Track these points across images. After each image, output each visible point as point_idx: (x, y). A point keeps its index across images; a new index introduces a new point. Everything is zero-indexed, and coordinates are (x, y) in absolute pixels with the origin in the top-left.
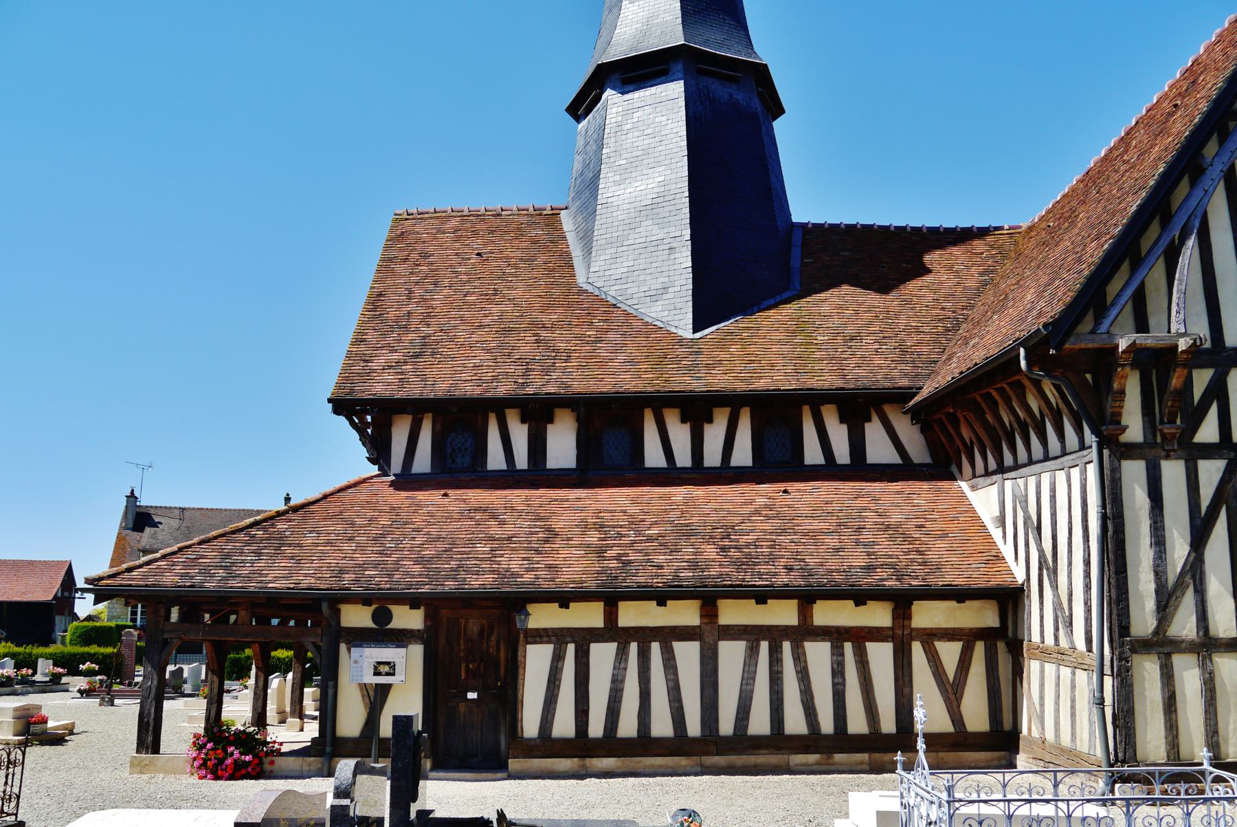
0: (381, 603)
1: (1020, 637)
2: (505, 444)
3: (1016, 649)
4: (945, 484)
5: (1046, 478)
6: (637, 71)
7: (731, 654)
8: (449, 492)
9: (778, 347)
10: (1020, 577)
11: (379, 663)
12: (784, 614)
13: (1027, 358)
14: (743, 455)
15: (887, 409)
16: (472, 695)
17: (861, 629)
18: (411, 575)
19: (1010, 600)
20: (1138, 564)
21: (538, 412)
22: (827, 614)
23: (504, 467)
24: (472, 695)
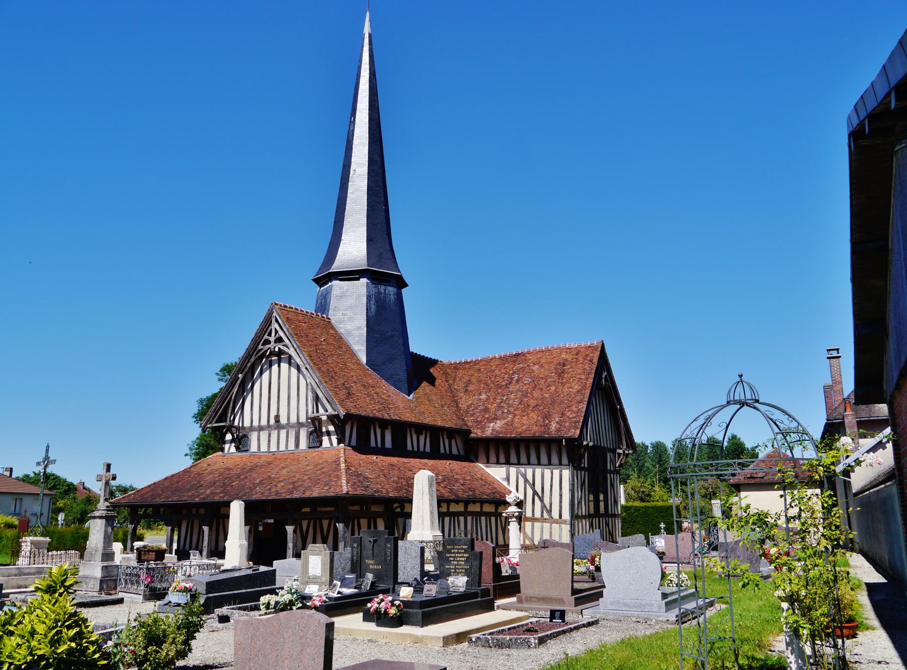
2: (444, 445)
4: (472, 464)
7: (469, 518)
22: (473, 508)
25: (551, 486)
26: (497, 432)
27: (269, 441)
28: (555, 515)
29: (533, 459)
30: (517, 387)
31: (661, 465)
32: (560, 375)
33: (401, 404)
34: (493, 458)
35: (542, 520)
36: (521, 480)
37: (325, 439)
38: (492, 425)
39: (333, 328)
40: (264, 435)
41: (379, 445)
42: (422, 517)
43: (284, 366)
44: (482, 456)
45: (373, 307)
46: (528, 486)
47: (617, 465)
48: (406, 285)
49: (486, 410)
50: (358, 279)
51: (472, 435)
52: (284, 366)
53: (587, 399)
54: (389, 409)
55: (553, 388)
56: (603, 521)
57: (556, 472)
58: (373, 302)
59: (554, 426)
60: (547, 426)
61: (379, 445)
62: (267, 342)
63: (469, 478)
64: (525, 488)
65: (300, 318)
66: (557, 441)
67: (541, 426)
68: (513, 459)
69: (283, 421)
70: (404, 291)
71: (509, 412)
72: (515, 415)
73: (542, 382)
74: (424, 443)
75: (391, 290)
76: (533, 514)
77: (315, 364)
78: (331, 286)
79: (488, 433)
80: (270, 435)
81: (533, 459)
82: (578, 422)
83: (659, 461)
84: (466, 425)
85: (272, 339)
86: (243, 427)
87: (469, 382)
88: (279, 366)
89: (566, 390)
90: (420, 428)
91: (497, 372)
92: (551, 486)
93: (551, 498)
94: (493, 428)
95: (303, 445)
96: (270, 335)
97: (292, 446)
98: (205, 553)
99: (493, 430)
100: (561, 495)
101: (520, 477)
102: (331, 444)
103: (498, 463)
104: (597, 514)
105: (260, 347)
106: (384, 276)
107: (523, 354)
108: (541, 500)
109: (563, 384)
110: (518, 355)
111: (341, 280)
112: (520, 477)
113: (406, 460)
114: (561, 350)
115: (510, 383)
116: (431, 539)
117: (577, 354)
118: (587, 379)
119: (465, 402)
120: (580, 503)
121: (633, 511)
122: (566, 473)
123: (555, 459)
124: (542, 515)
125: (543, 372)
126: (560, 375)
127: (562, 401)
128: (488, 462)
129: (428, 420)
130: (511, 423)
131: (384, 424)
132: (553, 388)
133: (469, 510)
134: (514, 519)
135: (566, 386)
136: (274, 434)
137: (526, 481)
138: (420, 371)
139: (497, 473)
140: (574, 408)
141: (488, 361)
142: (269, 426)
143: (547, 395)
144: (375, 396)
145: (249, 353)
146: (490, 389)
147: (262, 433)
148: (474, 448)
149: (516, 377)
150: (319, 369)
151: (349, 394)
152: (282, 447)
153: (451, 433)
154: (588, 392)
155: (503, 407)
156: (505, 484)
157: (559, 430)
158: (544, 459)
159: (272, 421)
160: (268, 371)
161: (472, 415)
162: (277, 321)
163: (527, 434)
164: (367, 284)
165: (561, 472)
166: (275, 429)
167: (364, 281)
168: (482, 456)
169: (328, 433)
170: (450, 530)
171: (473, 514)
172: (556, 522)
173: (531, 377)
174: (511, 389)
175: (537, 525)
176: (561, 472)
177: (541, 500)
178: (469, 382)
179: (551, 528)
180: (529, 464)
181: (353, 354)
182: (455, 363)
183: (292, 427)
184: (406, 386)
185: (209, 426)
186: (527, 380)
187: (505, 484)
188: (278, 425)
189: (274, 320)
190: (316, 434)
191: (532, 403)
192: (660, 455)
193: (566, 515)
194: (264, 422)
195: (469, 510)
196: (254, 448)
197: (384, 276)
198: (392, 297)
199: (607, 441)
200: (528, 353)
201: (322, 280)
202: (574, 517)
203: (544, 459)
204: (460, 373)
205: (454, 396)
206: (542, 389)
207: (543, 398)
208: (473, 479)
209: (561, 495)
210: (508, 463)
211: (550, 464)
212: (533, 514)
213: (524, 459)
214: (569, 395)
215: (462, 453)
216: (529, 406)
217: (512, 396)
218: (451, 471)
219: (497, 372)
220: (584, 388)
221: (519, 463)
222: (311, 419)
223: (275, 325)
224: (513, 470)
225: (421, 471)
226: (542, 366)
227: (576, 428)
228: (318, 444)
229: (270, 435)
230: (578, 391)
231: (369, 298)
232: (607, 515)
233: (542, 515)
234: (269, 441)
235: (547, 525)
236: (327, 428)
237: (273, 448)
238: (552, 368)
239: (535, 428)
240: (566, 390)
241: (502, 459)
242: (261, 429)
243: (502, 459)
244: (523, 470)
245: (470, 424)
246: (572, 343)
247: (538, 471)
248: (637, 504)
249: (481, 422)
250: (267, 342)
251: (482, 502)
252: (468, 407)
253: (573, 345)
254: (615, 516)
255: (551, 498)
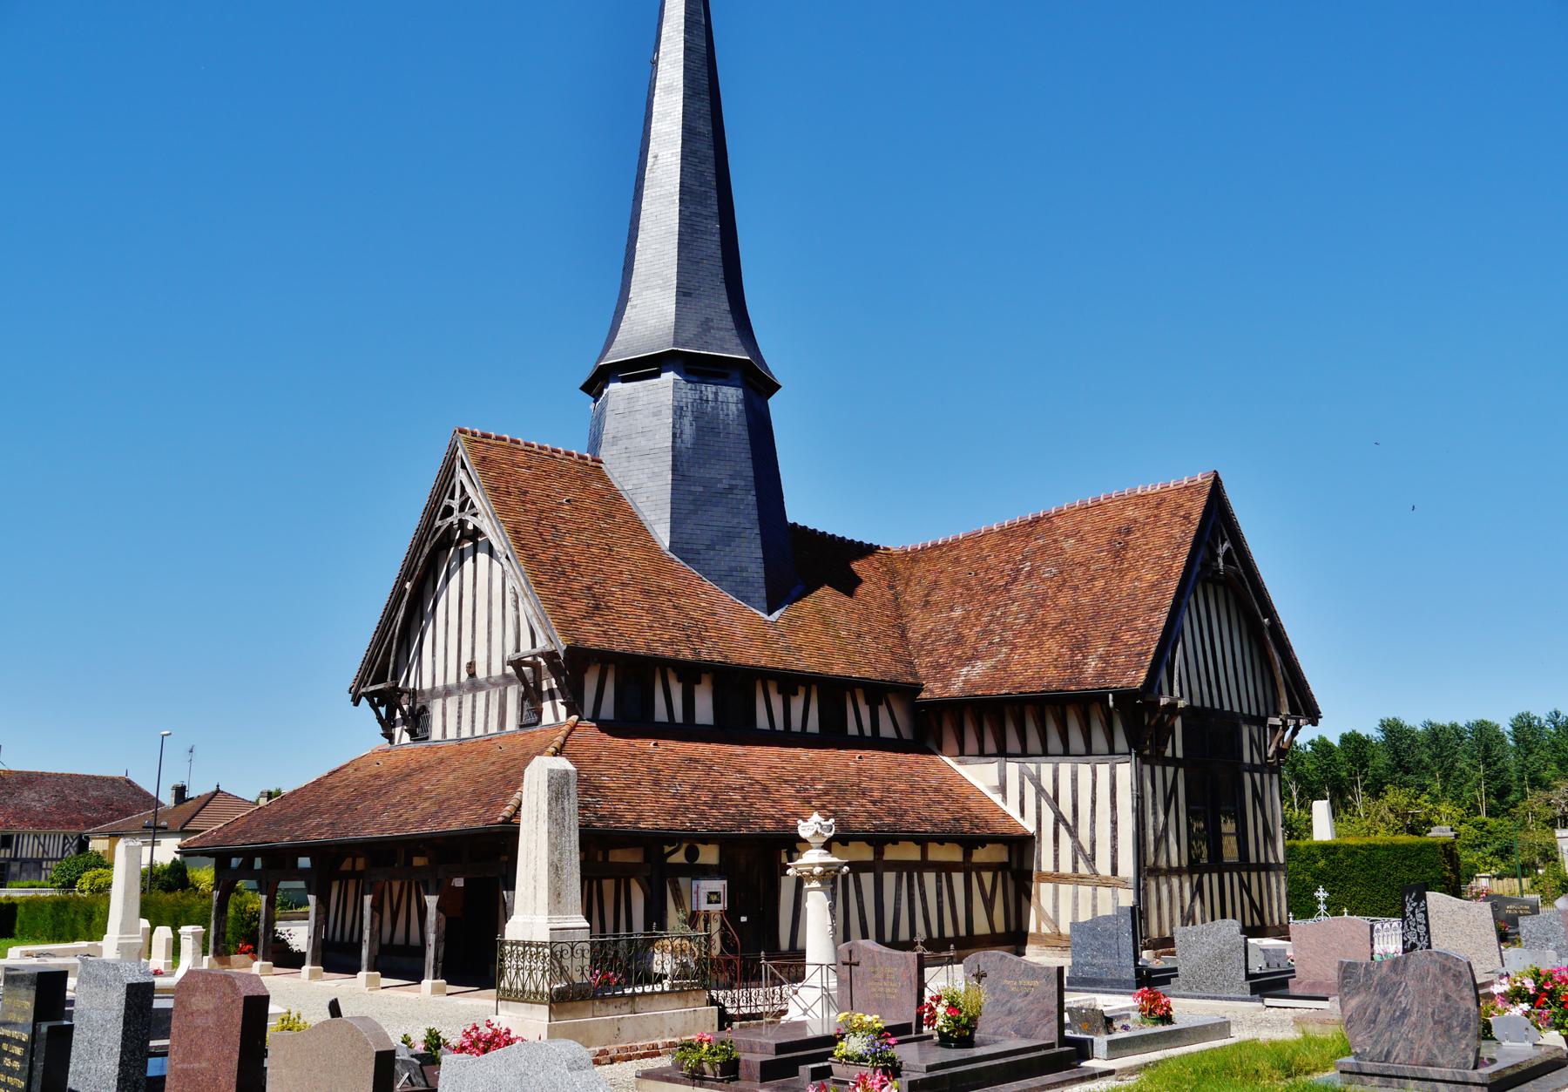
0: (693, 840)
1: (1026, 867)
2: (857, 717)
3: (1028, 875)
4: (925, 758)
5: (451, 734)
6: (642, 368)
7: (889, 878)
9: (746, 631)
10: (1032, 829)
15: (670, 671)
18: (715, 820)
19: (1022, 845)
20: (127, 893)
22: (938, 853)
25: (1094, 802)
26: (975, 686)
27: (460, 717)
28: (1103, 867)
29: (1054, 743)
31: (1488, 766)
32: (1118, 555)
33: (739, 630)
34: (971, 743)
35: (1076, 879)
36: (1030, 791)
37: (547, 706)
40: (452, 702)
41: (679, 718)
42: (535, 878)
43: (483, 557)
44: (950, 741)
45: (688, 430)
47: (1270, 752)
48: (775, 387)
49: (959, 640)
50: (656, 375)
51: (923, 695)
52: (483, 557)
53: (1170, 602)
55: (1100, 583)
56: (1232, 880)
57: (1103, 771)
58: (687, 421)
59: (1092, 665)
60: (1077, 667)
61: (679, 718)
62: (449, 511)
63: (902, 787)
64: (1039, 808)
65: (520, 458)
66: (1099, 697)
67: (1065, 667)
68: (1013, 744)
69: (481, 673)
71: (1003, 642)
72: (1015, 647)
73: (1079, 572)
74: (805, 713)
75: (731, 395)
79: (956, 689)
81: (1054, 743)
83: (1484, 759)
84: (915, 675)
85: (455, 504)
86: (422, 692)
88: (475, 560)
89: (1126, 586)
90: (789, 682)
91: (992, 561)
92: (1094, 802)
93: (1093, 829)
94: (967, 678)
95: (512, 724)
96: (452, 497)
97: (493, 728)
98: (260, 952)
99: (965, 682)
100: (1114, 823)
101: (1027, 783)
102: (557, 718)
103: (982, 754)
104: (1217, 864)
105: (438, 523)
106: (726, 373)
107: (1048, 518)
108: (1073, 832)
110: (1037, 520)
111: (624, 380)
112: (1027, 783)
113: (739, 750)
114: (1125, 501)
115: (1015, 580)
117: (1158, 506)
118: (1175, 556)
119: (920, 624)
120: (1161, 838)
122: (1125, 772)
123: (1099, 741)
124: (1075, 869)
125: (1084, 551)
126: (1118, 555)
128: (962, 753)
129: (806, 663)
130: (1006, 664)
131: (690, 673)
132: (1100, 583)
134: (816, 884)
135: (1127, 578)
136: (468, 699)
137: (1040, 791)
138: (812, 564)
139: (979, 775)
140: (1140, 624)
141: (976, 539)
142: (459, 685)
143: (1084, 600)
144: (672, 613)
145: (420, 539)
146: (972, 597)
148: (935, 724)
149: (1027, 566)
150: (531, 558)
151: (597, 607)
153: (876, 692)
154: (1173, 585)
155: (992, 632)
156: (997, 798)
157: (1101, 674)
158: (1076, 741)
159: (464, 676)
161: (930, 653)
163: (1035, 687)
164: (676, 382)
165: (1113, 769)
166: (469, 690)
167: (669, 377)
168: (950, 741)
170: (939, 894)
171: (899, 866)
173: (1057, 565)
174: (1013, 593)
175: (1066, 890)
176: (1113, 769)
177: (1073, 832)
179: (1094, 897)
180: (1045, 753)
182: (914, 550)
183: (495, 685)
184: (763, 592)
186: (1049, 571)
187: (997, 798)
188: (474, 685)
189: (458, 464)
190: (532, 698)
191: (1053, 618)
192: (1487, 748)
193: (1127, 868)
194: (452, 680)
196: (436, 734)
197: (726, 373)
198: (733, 408)
199: (1238, 695)
200: (1059, 514)
201: (595, 385)
202: (1146, 871)
203: (1076, 741)
205: (900, 617)
206: (1076, 588)
207: (1077, 607)
208: (913, 788)
209: (1114, 823)
210: (1002, 753)
211: (1089, 752)
213: (1034, 743)
214: (1132, 596)
215: (907, 734)
216: (1045, 625)
217: (1014, 608)
218: (859, 771)
220: (1166, 577)
221: (1024, 753)
222: (511, 663)
223: (461, 476)
224: (1013, 768)
226: (1082, 540)
227: (1139, 667)
228: (534, 719)
230: (1153, 586)
232: (1243, 864)
233: (1075, 869)
234: (460, 717)
235: (1085, 891)
236: (549, 684)
237: (466, 733)
238: (1103, 541)
239: (1052, 672)
240: (1126, 586)
242: (447, 692)
243: (990, 746)
244: (1032, 767)
245: (922, 672)
246: (1151, 486)
247: (1065, 769)
248: (1404, 839)
249: (944, 666)
250: (449, 511)
251: (922, 841)
252: (925, 637)
253: (1152, 487)
255: (1093, 829)
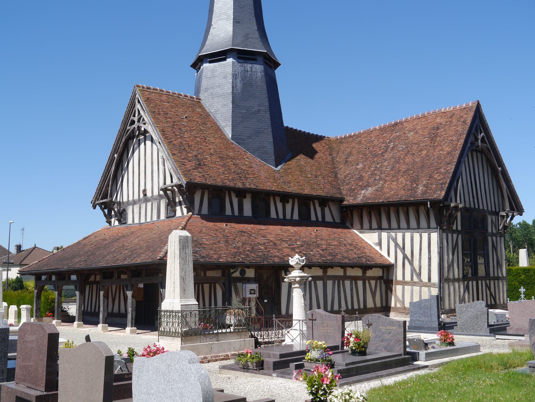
0: (244, 267)
2: (276, 209)
4: (345, 231)
6: (218, 57)
7: (330, 283)
8: (228, 224)
9: (266, 174)
10: (392, 261)
11: (251, 290)
12: (340, 272)
13: (430, 205)
14: (296, 217)
16: (266, 301)
17: (356, 276)
19: (388, 268)
21: (241, 193)
22: (351, 272)
23: (231, 214)
24: (266, 301)
25: (421, 250)
26: (368, 198)
28: (424, 278)
29: (403, 223)
30: (392, 154)
33: (263, 175)
34: (366, 224)
35: (412, 283)
37: (178, 208)
38: (363, 191)
39: (201, 107)
40: (136, 207)
43: (148, 143)
45: (239, 85)
46: (398, 250)
47: (501, 227)
49: (361, 178)
50: (225, 59)
51: (345, 203)
52: (148, 143)
53: (456, 160)
54: (247, 179)
55: (424, 152)
58: (238, 80)
60: (414, 190)
62: (133, 122)
64: (396, 252)
66: (423, 203)
67: (409, 190)
68: (385, 224)
69: (149, 194)
70: (277, 72)
73: (415, 147)
74: (292, 210)
75: (258, 69)
76: (404, 278)
77: (166, 138)
78: (203, 69)
79: (359, 200)
80: (140, 208)
81: (403, 223)
82: (445, 184)
84: (341, 194)
85: (136, 119)
87: (350, 154)
88: (145, 144)
89: (436, 153)
91: (376, 142)
94: (365, 195)
95: (163, 216)
96: (134, 116)
97: (155, 218)
98: (56, 316)
99: (363, 197)
102: (183, 213)
103: (371, 228)
105: (128, 128)
106: (256, 58)
107: (401, 123)
108: (411, 263)
109: (434, 147)
110: (396, 124)
111: (210, 62)
114: (436, 115)
115: (386, 151)
116: (179, 309)
118: (458, 140)
119: (343, 171)
121: (532, 273)
124: (412, 279)
127: (431, 164)
128: (362, 228)
129: (293, 189)
132: (424, 152)
133: (328, 274)
135: (437, 150)
136: (143, 206)
137: (397, 245)
138: (296, 144)
139: (370, 238)
140: (442, 170)
141: (369, 133)
143: (417, 160)
146: (367, 159)
147: (135, 206)
148: (349, 215)
150: (170, 143)
152: (149, 220)
153: (324, 201)
155: (376, 174)
156: (377, 248)
157: (425, 193)
159: (142, 195)
160: (138, 150)
161: (348, 184)
162: (139, 102)
163: (395, 199)
164: (233, 63)
166: (144, 202)
167: (230, 60)
169: (180, 204)
170: (352, 290)
171: (334, 278)
172: (425, 285)
173: (405, 144)
175: (408, 288)
177: (411, 263)
178: (350, 154)
179: (420, 291)
180: (399, 228)
181: (218, 129)
182: (341, 138)
183: (155, 199)
185: (97, 202)
187: (377, 248)
188: (146, 200)
189: (137, 101)
190: (171, 205)
191: (403, 168)
193: (435, 278)
194: (136, 197)
195: (328, 274)
196: (130, 221)
197: (256, 58)
198: (259, 74)
201: (197, 65)
204: (343, 147)
205: (334, 168)
206: (413, 154)
210: (380, 228)
211: (419, 228)
212: (404, 278)
213: (394, 224)
214: (439, 158)
216: (399, 171)
217: (386, 164)
218: (316, 237)
219: (376, 142)
220: (454, 149)
221: (390, 228)
222: (162, 190)
223: (138, 106)
224: (384, 235)
225: (174, 231)
228: (173, 214)
229: (140, 208)
230: (448, 153)
231: (235, 76)
233: (412, 279)
235: (416, 289)
237: (143, 221)
238: (426, 133)
239: (402, 192)
240: (436, 153)
241: (375, 225)
242: (134, 203)
243: (375, 225)
244: (393, 234)
245: (344, 192)
247: (408, 235)
250: (133, 122)
251: (344, 267)
252: (346, 177)
254: (498, 278)
